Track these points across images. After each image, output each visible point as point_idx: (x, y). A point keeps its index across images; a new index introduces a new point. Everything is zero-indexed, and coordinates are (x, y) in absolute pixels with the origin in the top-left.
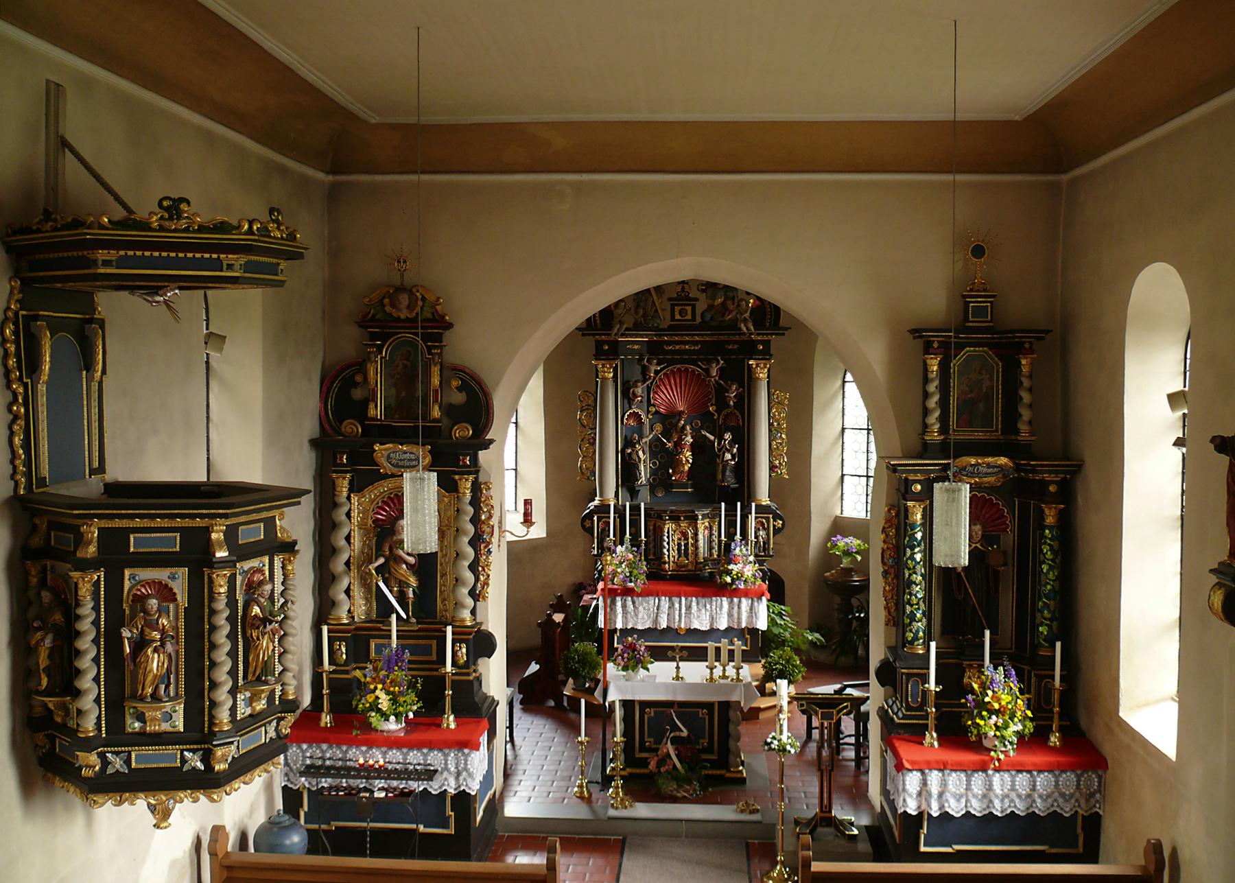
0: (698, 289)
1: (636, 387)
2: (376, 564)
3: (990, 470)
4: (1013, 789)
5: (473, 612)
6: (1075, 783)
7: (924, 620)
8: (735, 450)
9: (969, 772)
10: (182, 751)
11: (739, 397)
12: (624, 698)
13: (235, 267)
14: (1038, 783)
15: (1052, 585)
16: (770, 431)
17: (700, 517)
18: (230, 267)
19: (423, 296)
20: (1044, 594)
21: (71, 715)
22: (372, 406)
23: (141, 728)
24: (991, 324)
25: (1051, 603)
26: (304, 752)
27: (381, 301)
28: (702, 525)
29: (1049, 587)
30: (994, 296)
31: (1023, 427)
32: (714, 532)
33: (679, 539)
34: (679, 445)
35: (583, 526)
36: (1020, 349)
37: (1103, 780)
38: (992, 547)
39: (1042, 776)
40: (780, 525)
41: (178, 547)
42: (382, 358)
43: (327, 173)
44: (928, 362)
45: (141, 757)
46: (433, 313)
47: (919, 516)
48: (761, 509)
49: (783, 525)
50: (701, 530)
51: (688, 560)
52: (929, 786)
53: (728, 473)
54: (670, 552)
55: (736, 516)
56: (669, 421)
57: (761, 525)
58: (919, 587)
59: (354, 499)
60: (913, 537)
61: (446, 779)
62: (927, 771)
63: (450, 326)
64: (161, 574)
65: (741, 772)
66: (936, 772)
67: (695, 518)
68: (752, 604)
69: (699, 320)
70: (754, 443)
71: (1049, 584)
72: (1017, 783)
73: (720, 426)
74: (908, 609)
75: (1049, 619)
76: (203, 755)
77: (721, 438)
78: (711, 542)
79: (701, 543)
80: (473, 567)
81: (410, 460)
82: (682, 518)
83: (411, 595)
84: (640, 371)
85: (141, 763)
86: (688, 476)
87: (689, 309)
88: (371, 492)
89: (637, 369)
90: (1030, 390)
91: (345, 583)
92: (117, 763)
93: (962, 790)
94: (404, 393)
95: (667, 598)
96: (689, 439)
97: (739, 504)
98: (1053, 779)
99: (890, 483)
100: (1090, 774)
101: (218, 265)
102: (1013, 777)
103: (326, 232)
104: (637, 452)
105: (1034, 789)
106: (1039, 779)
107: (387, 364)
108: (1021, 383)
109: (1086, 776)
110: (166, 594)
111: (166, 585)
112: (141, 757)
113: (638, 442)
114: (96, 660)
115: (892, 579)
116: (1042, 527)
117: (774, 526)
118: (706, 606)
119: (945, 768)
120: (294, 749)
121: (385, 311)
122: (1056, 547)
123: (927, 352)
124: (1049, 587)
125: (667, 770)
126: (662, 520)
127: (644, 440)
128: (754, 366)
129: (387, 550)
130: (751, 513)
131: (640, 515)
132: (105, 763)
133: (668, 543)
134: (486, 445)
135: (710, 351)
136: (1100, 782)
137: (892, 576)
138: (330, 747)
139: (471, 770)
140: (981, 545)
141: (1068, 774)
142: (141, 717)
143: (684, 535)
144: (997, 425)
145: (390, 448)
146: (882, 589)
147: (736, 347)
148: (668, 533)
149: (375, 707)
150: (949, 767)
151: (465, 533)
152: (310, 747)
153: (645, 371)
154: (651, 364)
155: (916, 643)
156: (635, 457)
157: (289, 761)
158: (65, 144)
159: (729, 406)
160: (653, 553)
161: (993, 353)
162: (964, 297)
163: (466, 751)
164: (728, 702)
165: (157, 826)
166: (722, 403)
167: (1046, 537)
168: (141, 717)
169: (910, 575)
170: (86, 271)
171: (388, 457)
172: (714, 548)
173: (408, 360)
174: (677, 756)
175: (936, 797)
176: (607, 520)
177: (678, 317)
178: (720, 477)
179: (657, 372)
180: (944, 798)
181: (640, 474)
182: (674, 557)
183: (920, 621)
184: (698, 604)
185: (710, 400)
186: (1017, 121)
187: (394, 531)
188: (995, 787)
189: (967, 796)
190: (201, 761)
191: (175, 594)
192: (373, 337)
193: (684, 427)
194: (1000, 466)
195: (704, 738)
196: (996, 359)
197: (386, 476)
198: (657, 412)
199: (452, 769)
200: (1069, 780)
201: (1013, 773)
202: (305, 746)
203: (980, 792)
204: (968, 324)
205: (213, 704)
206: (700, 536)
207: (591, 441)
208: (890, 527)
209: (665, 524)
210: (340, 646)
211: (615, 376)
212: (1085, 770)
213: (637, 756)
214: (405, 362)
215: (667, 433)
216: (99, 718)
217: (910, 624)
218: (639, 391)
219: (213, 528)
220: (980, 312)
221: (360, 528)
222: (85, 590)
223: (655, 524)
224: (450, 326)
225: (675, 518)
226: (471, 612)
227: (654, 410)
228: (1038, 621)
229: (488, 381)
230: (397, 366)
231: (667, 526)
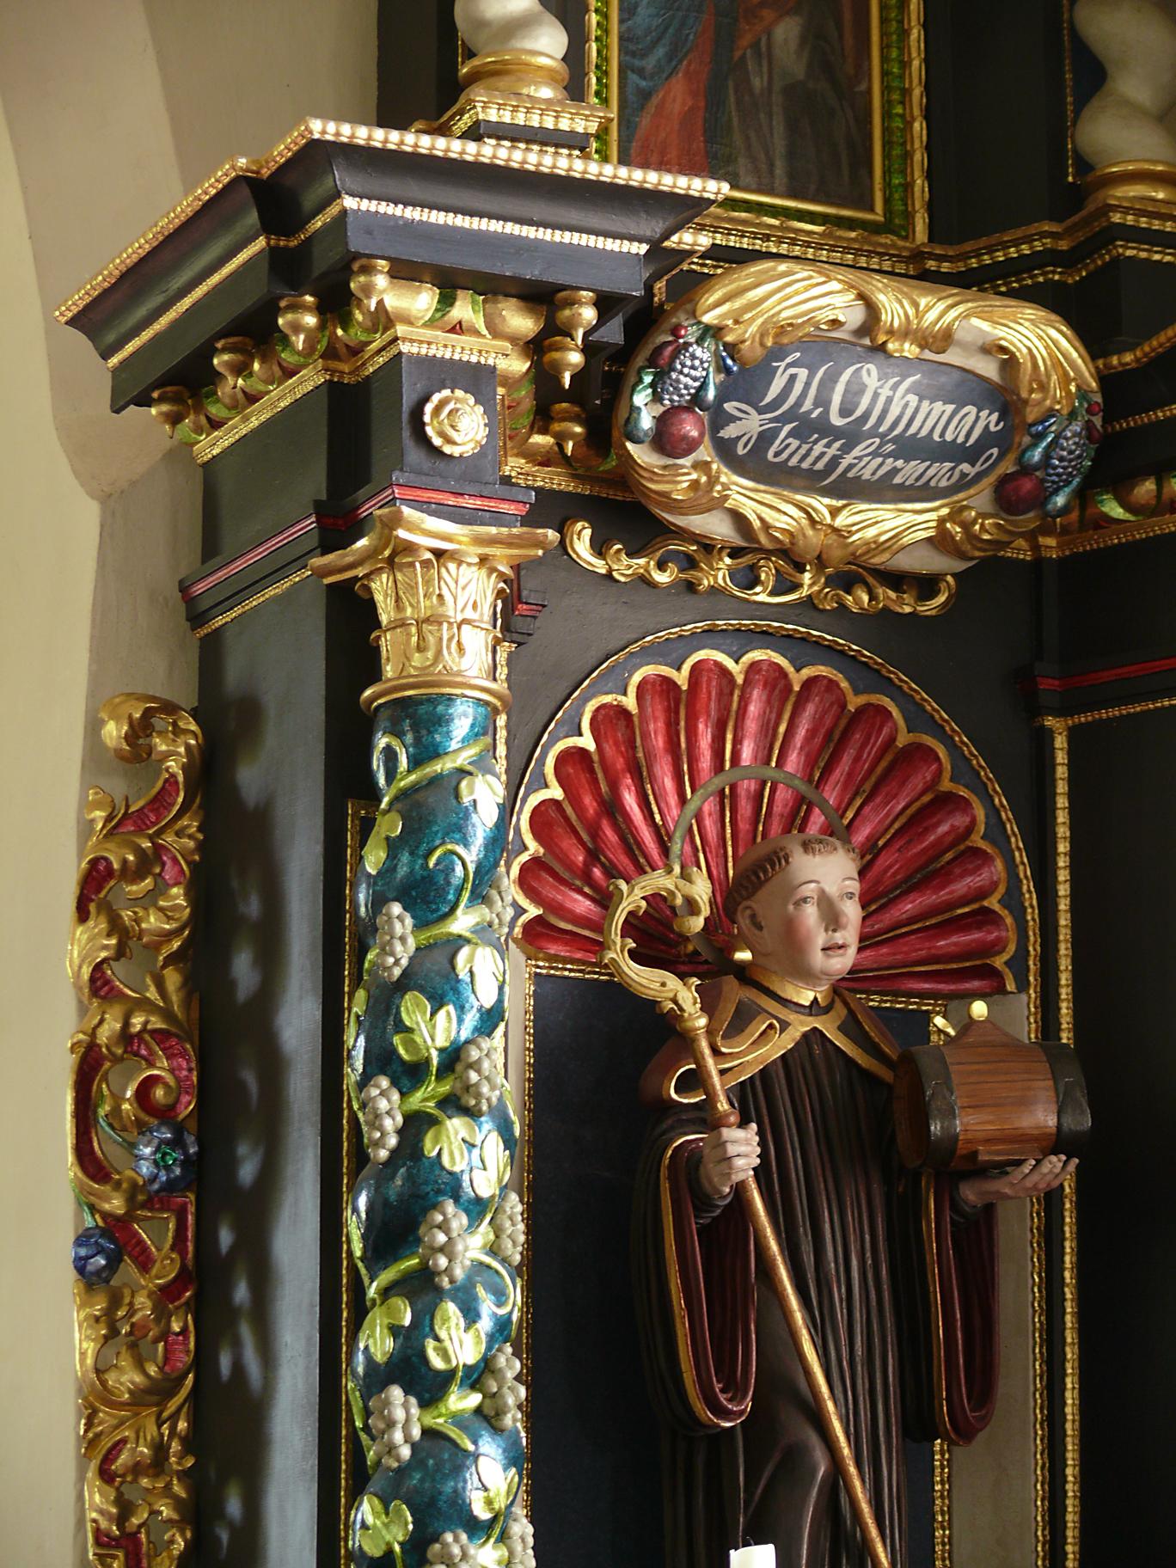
169: (416, 1125)
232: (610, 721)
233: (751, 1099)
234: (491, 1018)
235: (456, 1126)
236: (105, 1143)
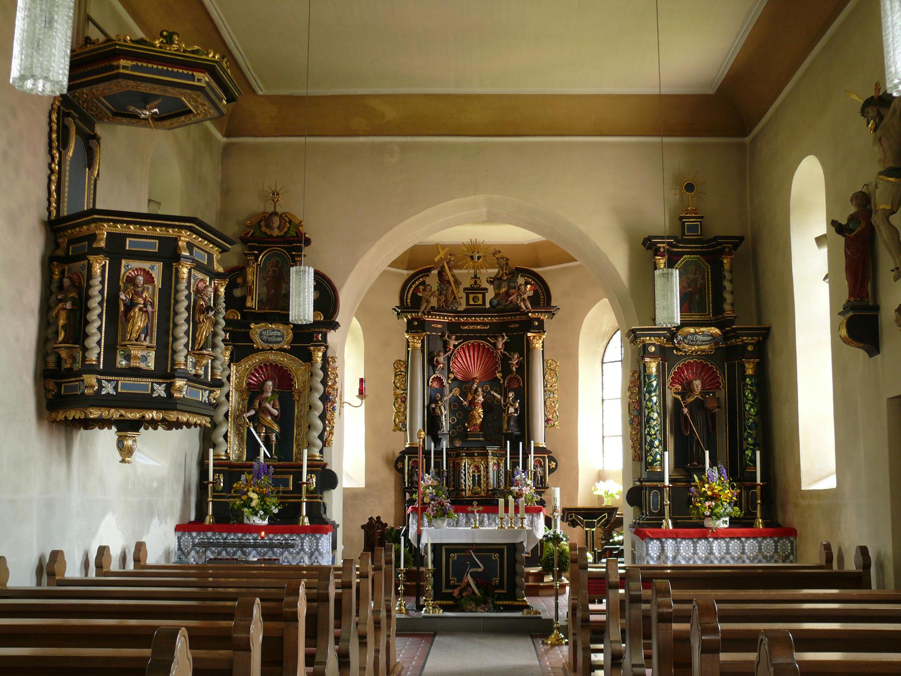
0: (487, 281)
1: (439, 356)
2: (249, 414)
3: (705, 338)
4: (728, 553)
5: (321, 452)
6: (774, 547)
7: (660, 447)
8: (517, 404)
10: (152, 383)
11: (520, 365)
12: (434, 542)
13: (202, 81)
14: (746, 548)
16: (545, 391)
17: (490, 454)
18: (199, 80)
19: (290, 220)
21: (77, 361)
22: (249, 298)
23: (126, 364)
24: (701, 237)
25: (753, 432)
26: (193, 538)
27: (260, 222)
28: (492, 462)
29: (751, 421)
30: (702, 217)
31: (727, 307)
32: (501, 468)
33: (474, 472)
34: (472, 403)
35: (396, 468)
36: (722, 252)
37: (794, 545)
38: (709, 395)
39: (749, 542)
40: (554, 466)
41: (157, 248)
42: (258, 265)
43: (224, 136)
44: (657, 262)
45: (126, 384)
46: (296, 233)
47: (654, 370)
48: (538, 450)
49: (556, 466)
50: (491, 464)
51: (481, 488)
52: (666, 551)
53: (512, 423)
54: (467, 482)
55: (519, 458)
56: (465, 385)
57: (539, 464)
58: (656, 422)
59: (233, 368)
60: (650, 385)
61: (302, 558)
62: (664, 540)
63: (308, 242)
64: (146, 265)
65: (525, 601)
66: (671, 541)
67: (486, 455)
68: (532, 518)
69: (488, 306)
70: (532, 398)
71: (751, 418)
72: (730, 548)
73: (505, 389)
74: (649, 438)
75: (752, 445)
76: (166, 387)
77: (506, 397)
78: (499, 477)
79: (491, 475)
80: (323, 417)
81: (277, 336)
82: (476, 454)
83: (274, 439)
84: (442, 345)
85: (124, 390)
86: (480, 428)
87: (480, 296)
88: (246, 362)
89: (440, 344)
90: (731, 281)
91: (223, 430)
92: (108, 389)
93: (690, 554)
94: (273, 291)
95: (464, 515)
96: (481, 399)
97: (521, 443)
98: (757, 545)
99: (632, 351)
100: (784, 540)
101: (192, 78)
102: (727, 543)
103: (220, 177)
104: (440, 407)
105: (743, 553)
106: (747, 545)
107: (262, 269)
108: (725, 277)
109: (781, 542)
110: (149, 279)
111: (148, 272)
112: (126, 384)
113: (441, 400)
114: (100, 316)
115: (637, 425)
116: (744, 377)
117: (549, 466)
118: (495, 521)
119: (677, 537)
120: (186, 536)
121: (262, 231)
123: (656, 255)
124: (751, 421)
125: (468, 595)
126: (460, 456)
127: (445, 398)
128: (531, 338)
129: (257, 404)
130: (530, 454)
131: (442, 458)
132: (101, 387)
133: (465, 475)
134: (335, 326)
135: (496, 330)
136: (792, 546)
138: (214, 535)
139: (322, 550)
140: (701, 396)
141: (768, 540)
142: (128, 357)
143: (477, 468)
144: (709, 310)
145: (262, 327)
146: (630, 434)
147: (517, 325)
148: (465, 466)
149: (247, 503)
151: (317, 390)
152: (198, 535)
153: (445, 344)
154: (451, 339)
155: (655, 464)
156: (438, 411)
157: (182, 547)
158: (89, 19)
159: (511, 371)
160: (452, 480)
162: (681, 218)
163: (318, 536)
164: (514, 545)
165: (123, 461)
166: (506, 370)
167: (747, 384)
168: (128, 357)
169: (649, 413)
170: (111, 73)
171: (261, 334)
172: (501, 481)
173: (276, 267)
174: (476, 585)
175: (671, 559)
176: (416, 459)
177: (471, 302)
178: (505, 426)
179: (455, 346)
180: (677, 560)
181: (442, 424)
182: (470, 486)
183: (658, 447)
184: (489, 519)
185: (497, 368)
186: (711, 95)
187: (263, 391)
188: (715, 551)
189: (694, 559)
190: (164, 391)
191: (153, 278)
192: (251, 248)
193: (476, 390)
194: (712, 335)
195: (496, 577)
196: (706, 263)
197: (258, 350)
198: (455, 379)
199: (307, 550)
200: (769, 545)
201: (728, 540)
202: (194, 534)
203: (704, 555)
204: (684, 237)
205: (174, 352)
206: (491, 469)
207: (403, 399)
208: (634, 386)
209: (462, 459)
210: (219, 476)
211: (423, 346)
212: (781, 537)
213: (443, 592)
214: (274, 268)
215: (464, 394)
216: (99, 354)
218: (441, 359)
219: (180, 239)
220: (693, 228)
221: (236, 390)
222: (97, 269)
223: (454, 462)
224: (308, 242)
225: (470, 455)
226: (320, 452)
227: (453, 376)
228: (745, 447)
229: (337, 285)
230: (268, 272)
231: (464, 461)
232: (679, 368)
233: (232, 572)
234: (655, 403)
235: (652, 413)
236: (632, 412)
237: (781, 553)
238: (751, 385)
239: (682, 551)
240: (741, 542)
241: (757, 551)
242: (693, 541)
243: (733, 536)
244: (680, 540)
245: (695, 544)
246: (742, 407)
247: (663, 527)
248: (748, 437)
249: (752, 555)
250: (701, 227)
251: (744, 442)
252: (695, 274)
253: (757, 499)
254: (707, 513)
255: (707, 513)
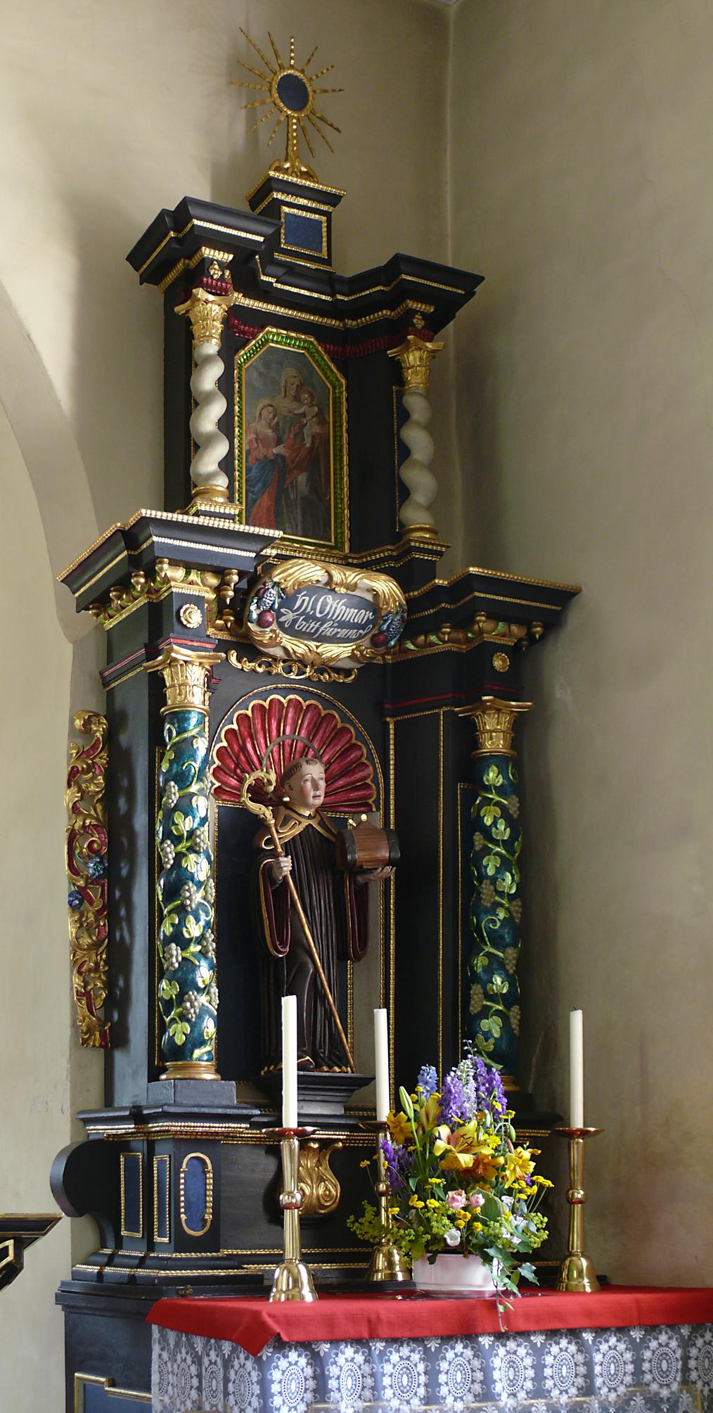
9: (433, 1345)
15: (507, 909)
20: (490, 932)
36: (397, 332)
52: (334, 1395)
62: (325, 1348)
66: (349, 1351)
71: (502, 905)
102: (538, 1353)
119: (374, 1336)
122: (514, 811)
124: (502, 915)
137: (98, 905)
140: (321, 824)
141: (663, 1338)
150: (384, 1331)
161: (327, 352)
167: (488, 789)
169: (179, 856)
183: (205, 990)
201: (538, 1340)
217: (181, 997)
232: (243, 719)
234: (204, 820)
235: (192, 857)
237: (699, 1385)
238: (500, 791)
239: (388, 1393)
240: (582, 1347)
241: (628, 1379)
242: (426, 1350)
243: (557, 1325)
244: (380, 1345)
245: (431, 1359)
246: (474, 860)
247: (279, 1294)
248: (489, 971)
249: (612, 1396)
250: (329, 227)
251: (476, 990)
252: (297, 398)
253: (572, 1186)
254: (453, 1237)
255: (453, 1237)
